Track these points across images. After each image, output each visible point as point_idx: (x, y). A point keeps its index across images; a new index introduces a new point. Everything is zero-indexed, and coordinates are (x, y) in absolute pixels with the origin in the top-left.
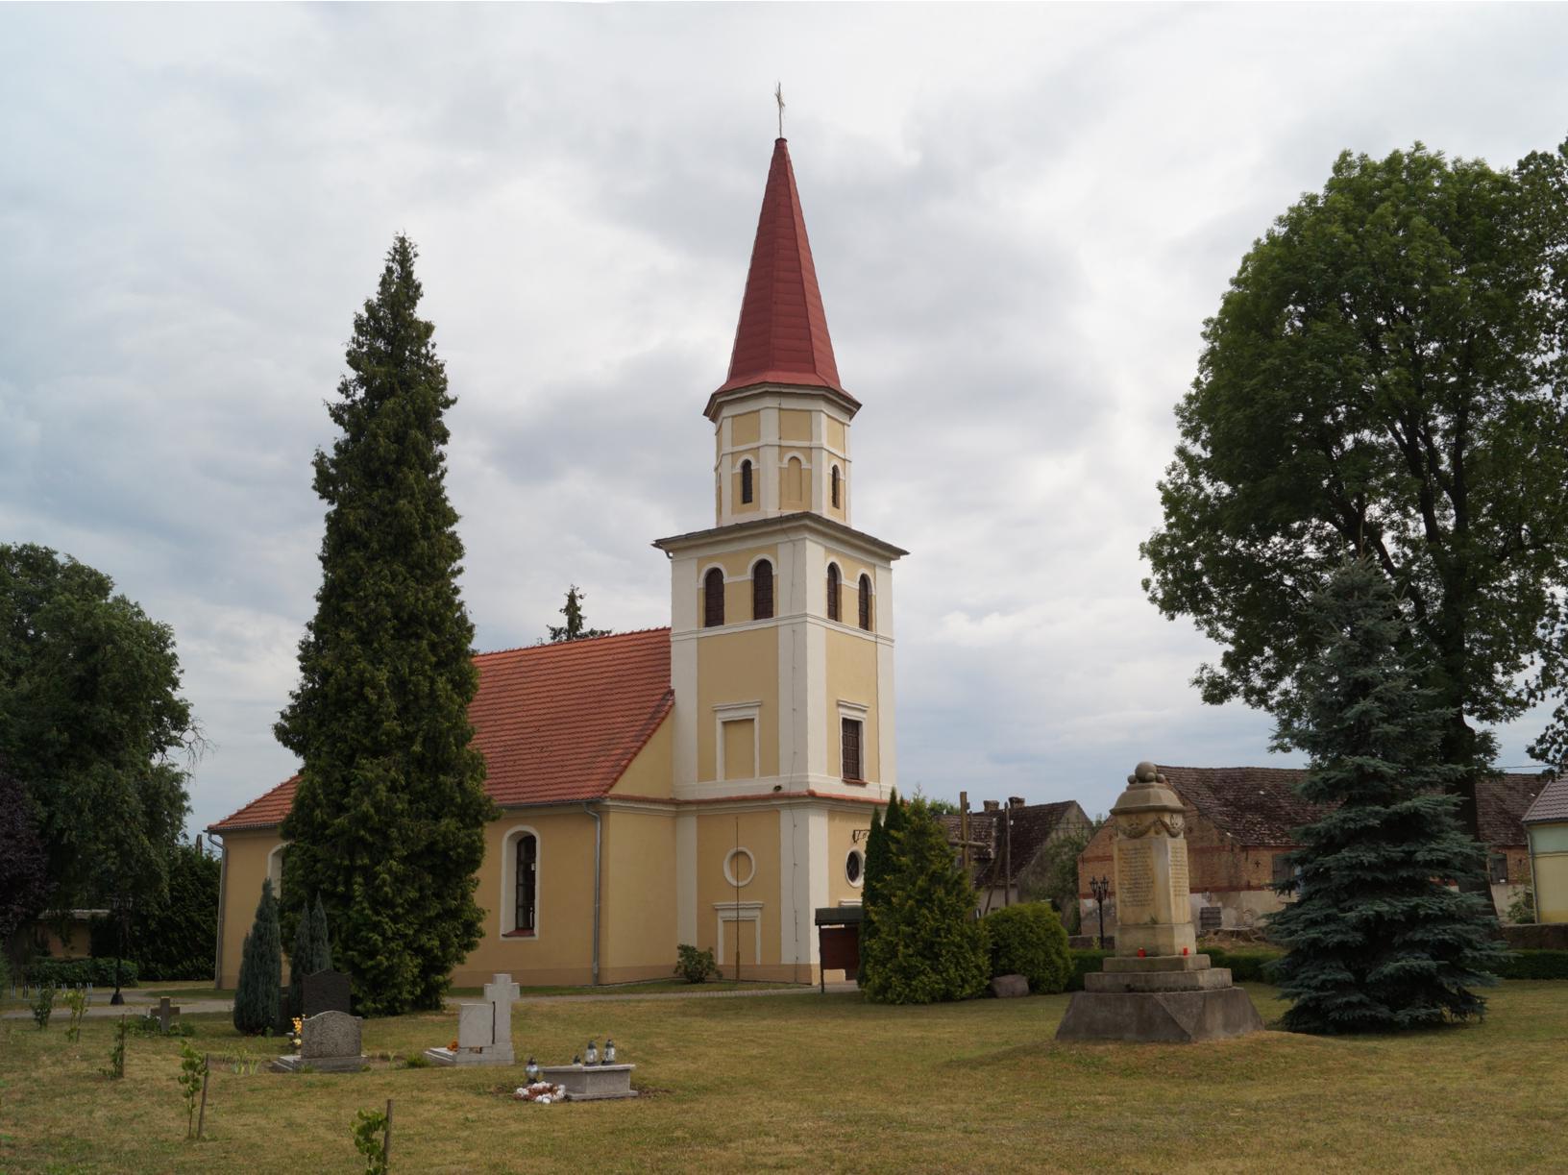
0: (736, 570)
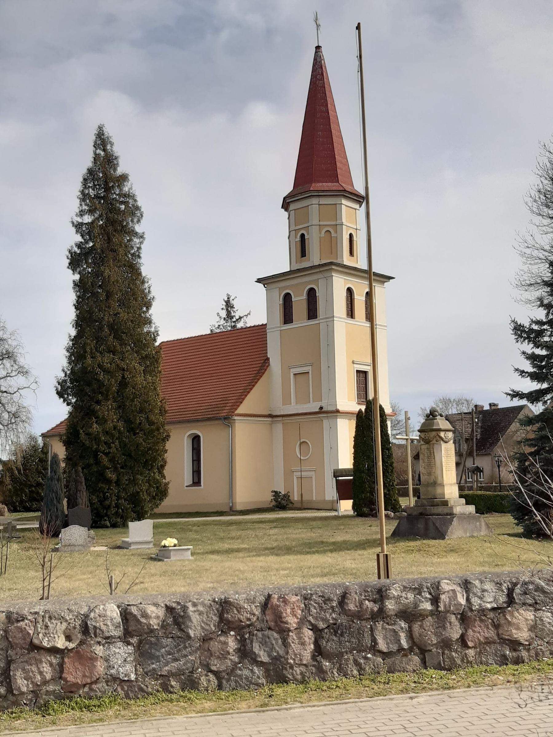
0: (299, 296)
